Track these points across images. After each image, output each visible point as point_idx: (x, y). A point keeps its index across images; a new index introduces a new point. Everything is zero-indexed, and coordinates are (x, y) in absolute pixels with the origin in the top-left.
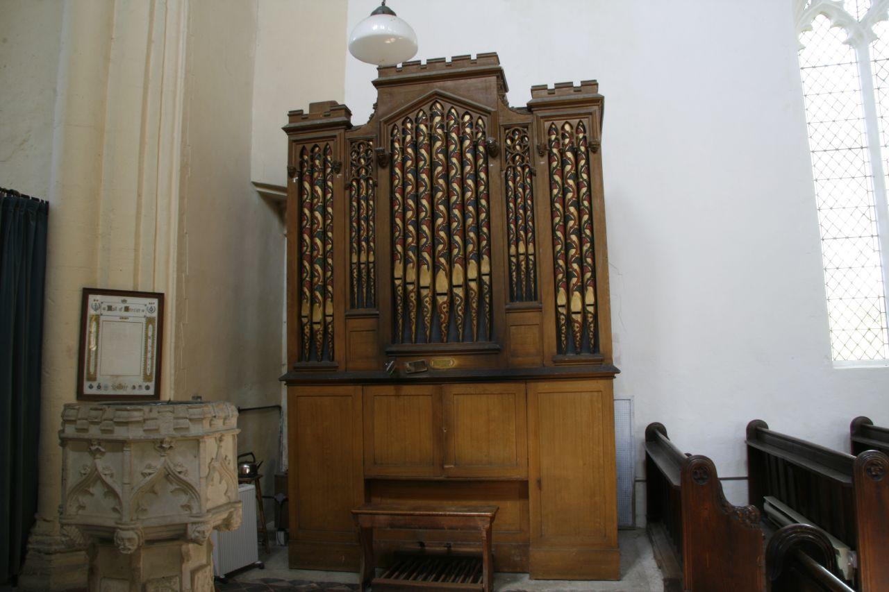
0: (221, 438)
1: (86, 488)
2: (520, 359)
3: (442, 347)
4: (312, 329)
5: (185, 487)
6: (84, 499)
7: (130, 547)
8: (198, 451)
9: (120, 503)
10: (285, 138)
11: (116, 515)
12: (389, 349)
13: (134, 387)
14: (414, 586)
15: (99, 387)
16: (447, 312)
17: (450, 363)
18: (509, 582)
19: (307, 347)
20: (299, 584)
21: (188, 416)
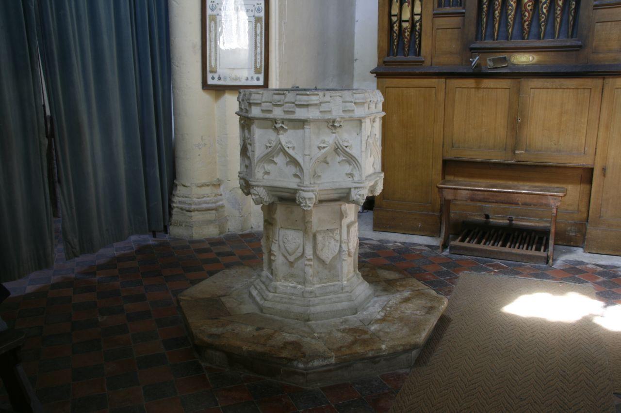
0: (374, 119)
1: (271, 158)
2: (601, 56)
3: (523, 44)
4: (400, 26)
5: (350, 159)
6: (269, 167)
7: (309, 205)
8: (361, 129)
9: (301, 170)
11: (297, 180)
12: (473, 46)
13: (247, 79)
14: (487, 250)
15: (219, 78)
16: (531, 10)
17: (524, 59)
18: (565, 253)
19: (395, 44)
20: (386, 243)
21: (353, 100)
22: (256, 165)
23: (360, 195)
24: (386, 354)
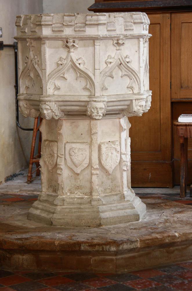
5: (130, 73)
9: (92, 83)
22: (48, 82)
23: (140, 106)
24: (180, 240)
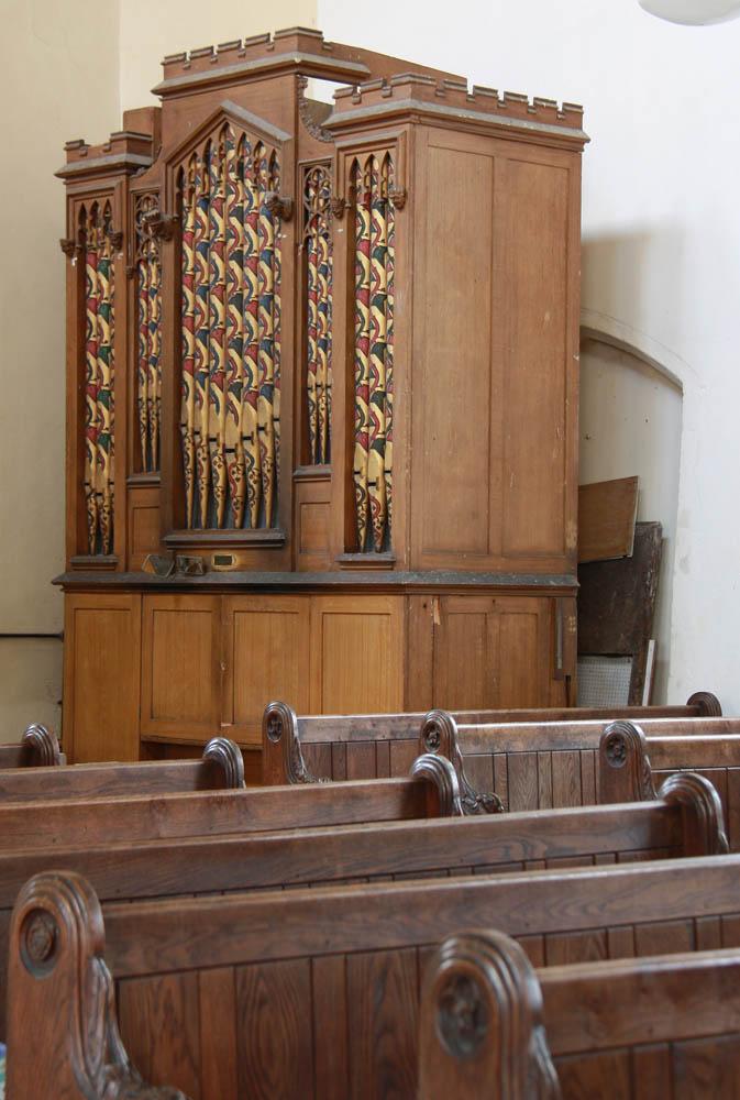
10: (60, 189)
